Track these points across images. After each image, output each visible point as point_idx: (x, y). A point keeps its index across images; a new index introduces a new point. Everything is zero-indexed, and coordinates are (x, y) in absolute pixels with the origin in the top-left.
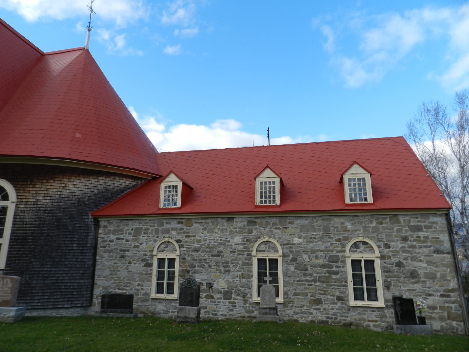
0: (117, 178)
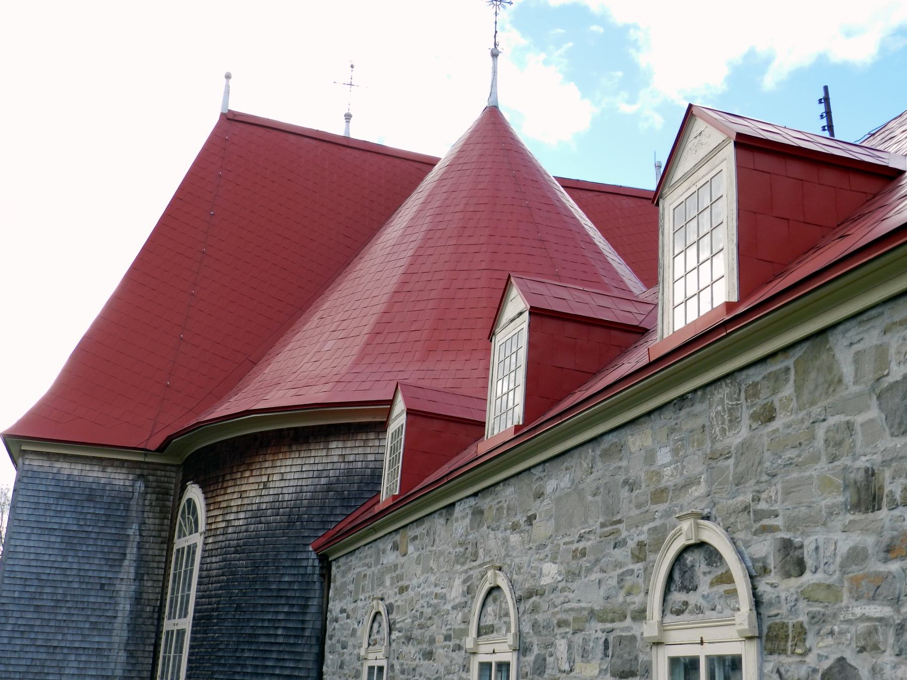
0: (372, 436)
